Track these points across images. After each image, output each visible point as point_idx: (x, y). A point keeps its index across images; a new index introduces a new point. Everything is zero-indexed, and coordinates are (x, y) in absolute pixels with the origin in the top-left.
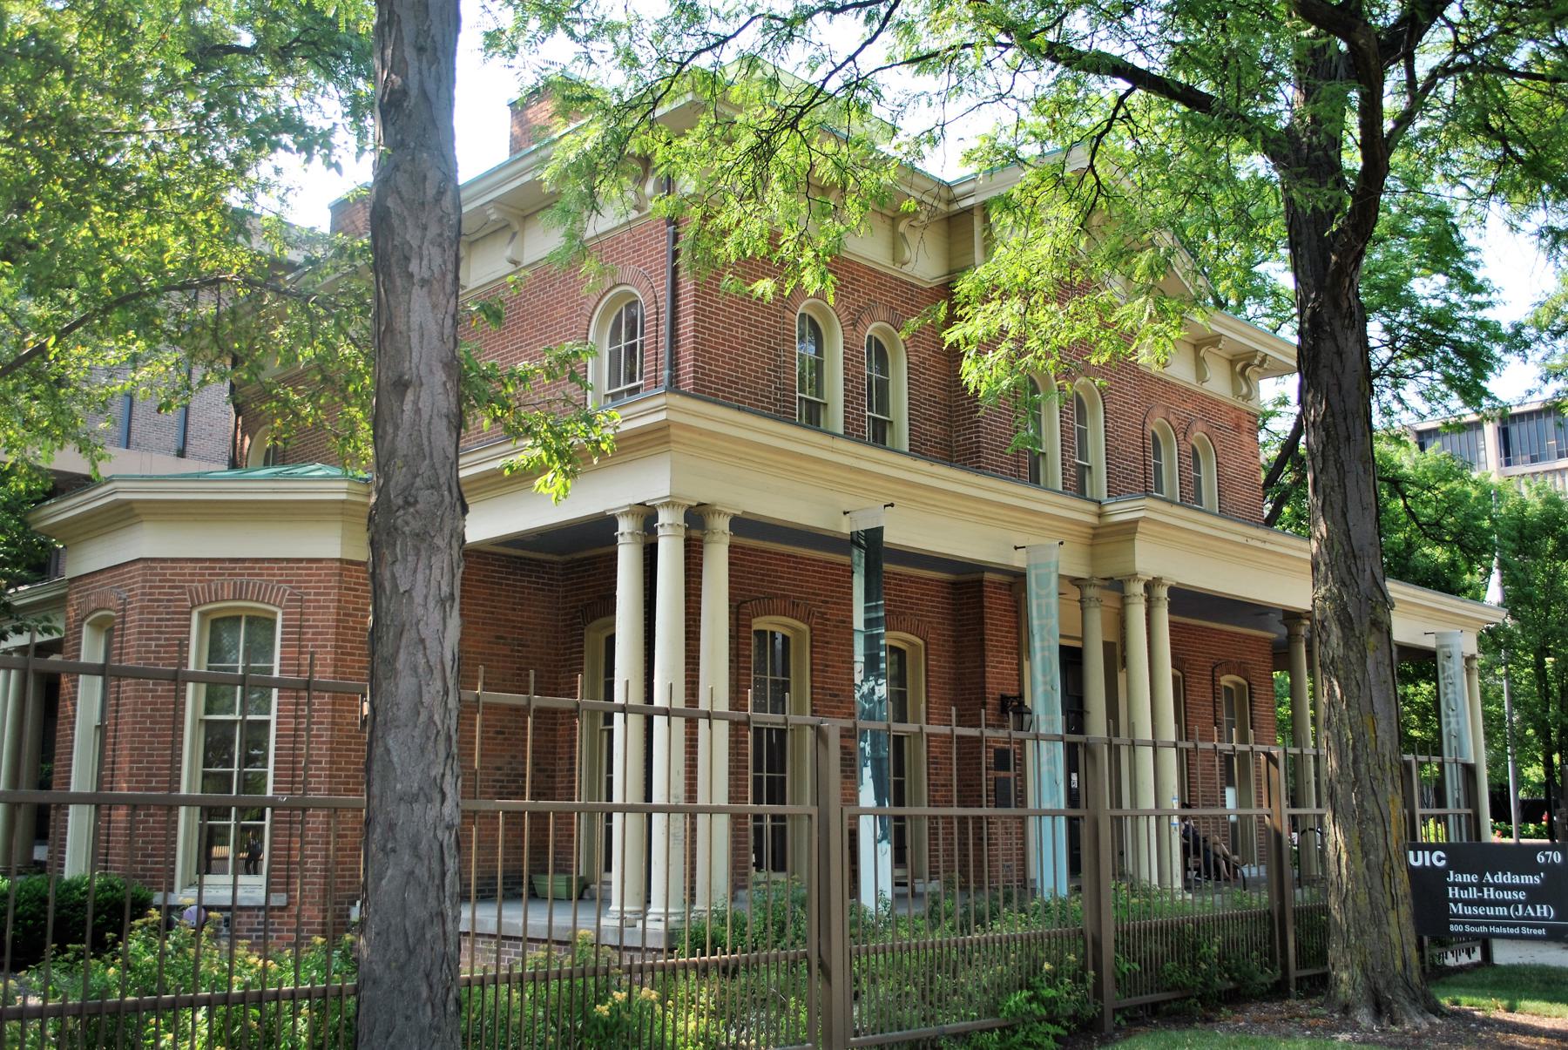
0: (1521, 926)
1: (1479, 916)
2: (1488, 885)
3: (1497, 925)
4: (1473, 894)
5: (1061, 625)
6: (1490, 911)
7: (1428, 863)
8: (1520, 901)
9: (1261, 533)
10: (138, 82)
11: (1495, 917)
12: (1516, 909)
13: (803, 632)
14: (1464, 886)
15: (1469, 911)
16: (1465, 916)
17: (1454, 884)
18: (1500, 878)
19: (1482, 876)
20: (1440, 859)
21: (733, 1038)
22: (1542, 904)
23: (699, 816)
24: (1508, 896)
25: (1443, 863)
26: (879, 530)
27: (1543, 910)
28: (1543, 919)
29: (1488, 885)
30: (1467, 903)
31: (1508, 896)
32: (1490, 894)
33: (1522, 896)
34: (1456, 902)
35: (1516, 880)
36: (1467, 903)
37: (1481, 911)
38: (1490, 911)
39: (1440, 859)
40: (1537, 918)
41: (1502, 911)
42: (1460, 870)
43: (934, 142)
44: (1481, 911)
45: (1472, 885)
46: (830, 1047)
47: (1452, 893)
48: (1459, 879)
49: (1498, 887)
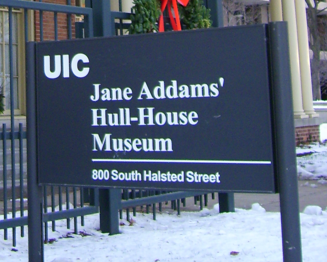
1: (132, 154)
2: (146, 103)
3: (154, 168)
4: (124, 118)
7: (66, 75)
9: (202, 211)
10: (129, 30)
14: (113, 107)
15: (119, 145)
16: (112, 154)
17: (100, 104)
18: (163, 91)
19: (137, 90)
20: (81, 65)
23: (29, 11)
25: (86, 71)
29: (146, 103)
30: (118, 132)
32: (148, 117)
34: (102, 131)
35: (185, 92)
36: (118, 132)
37: (132, 145)
38: (147, 145)
39: (81, 65)
42: (107, 84)
43: (246, 254)
44: (132, 145)
45: (123, 104)
47: (99, 117)
48: (107, 95)
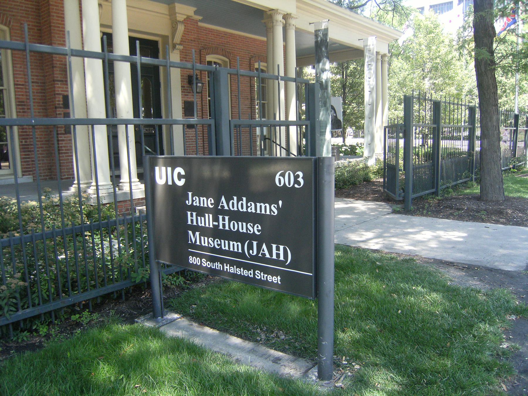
0: (255, 268)
2: (224, 212)
5: (129, 23)
6: (225, 245)
8: (253, 237)
11: (228, 253)
12: (250, 247)
13: (227, 62)
16: (201, 248)
17: (193, 208)
20: (180, 177)
21: (106, 244)
22: (278, 243)
24: (242, 227)
26: (326, 32)
27: (279, 252)
28: (277, 262)
29: (224, 212)
31: (242, 227)
32: (225, 223)
33: (256, 229)
38: (225, 245)
39: (180, 177)
40: (270, 261)
41: (235, 246)
42: (199, 194)
46: (527, 193)
49: (236, 216)
